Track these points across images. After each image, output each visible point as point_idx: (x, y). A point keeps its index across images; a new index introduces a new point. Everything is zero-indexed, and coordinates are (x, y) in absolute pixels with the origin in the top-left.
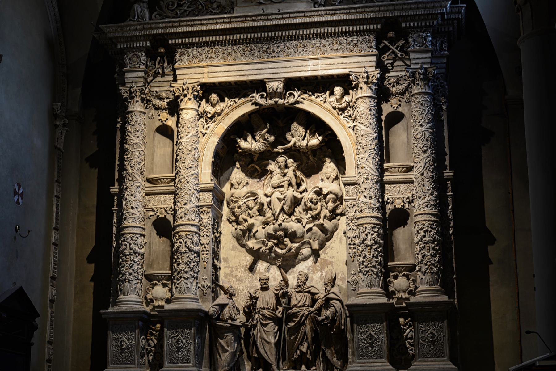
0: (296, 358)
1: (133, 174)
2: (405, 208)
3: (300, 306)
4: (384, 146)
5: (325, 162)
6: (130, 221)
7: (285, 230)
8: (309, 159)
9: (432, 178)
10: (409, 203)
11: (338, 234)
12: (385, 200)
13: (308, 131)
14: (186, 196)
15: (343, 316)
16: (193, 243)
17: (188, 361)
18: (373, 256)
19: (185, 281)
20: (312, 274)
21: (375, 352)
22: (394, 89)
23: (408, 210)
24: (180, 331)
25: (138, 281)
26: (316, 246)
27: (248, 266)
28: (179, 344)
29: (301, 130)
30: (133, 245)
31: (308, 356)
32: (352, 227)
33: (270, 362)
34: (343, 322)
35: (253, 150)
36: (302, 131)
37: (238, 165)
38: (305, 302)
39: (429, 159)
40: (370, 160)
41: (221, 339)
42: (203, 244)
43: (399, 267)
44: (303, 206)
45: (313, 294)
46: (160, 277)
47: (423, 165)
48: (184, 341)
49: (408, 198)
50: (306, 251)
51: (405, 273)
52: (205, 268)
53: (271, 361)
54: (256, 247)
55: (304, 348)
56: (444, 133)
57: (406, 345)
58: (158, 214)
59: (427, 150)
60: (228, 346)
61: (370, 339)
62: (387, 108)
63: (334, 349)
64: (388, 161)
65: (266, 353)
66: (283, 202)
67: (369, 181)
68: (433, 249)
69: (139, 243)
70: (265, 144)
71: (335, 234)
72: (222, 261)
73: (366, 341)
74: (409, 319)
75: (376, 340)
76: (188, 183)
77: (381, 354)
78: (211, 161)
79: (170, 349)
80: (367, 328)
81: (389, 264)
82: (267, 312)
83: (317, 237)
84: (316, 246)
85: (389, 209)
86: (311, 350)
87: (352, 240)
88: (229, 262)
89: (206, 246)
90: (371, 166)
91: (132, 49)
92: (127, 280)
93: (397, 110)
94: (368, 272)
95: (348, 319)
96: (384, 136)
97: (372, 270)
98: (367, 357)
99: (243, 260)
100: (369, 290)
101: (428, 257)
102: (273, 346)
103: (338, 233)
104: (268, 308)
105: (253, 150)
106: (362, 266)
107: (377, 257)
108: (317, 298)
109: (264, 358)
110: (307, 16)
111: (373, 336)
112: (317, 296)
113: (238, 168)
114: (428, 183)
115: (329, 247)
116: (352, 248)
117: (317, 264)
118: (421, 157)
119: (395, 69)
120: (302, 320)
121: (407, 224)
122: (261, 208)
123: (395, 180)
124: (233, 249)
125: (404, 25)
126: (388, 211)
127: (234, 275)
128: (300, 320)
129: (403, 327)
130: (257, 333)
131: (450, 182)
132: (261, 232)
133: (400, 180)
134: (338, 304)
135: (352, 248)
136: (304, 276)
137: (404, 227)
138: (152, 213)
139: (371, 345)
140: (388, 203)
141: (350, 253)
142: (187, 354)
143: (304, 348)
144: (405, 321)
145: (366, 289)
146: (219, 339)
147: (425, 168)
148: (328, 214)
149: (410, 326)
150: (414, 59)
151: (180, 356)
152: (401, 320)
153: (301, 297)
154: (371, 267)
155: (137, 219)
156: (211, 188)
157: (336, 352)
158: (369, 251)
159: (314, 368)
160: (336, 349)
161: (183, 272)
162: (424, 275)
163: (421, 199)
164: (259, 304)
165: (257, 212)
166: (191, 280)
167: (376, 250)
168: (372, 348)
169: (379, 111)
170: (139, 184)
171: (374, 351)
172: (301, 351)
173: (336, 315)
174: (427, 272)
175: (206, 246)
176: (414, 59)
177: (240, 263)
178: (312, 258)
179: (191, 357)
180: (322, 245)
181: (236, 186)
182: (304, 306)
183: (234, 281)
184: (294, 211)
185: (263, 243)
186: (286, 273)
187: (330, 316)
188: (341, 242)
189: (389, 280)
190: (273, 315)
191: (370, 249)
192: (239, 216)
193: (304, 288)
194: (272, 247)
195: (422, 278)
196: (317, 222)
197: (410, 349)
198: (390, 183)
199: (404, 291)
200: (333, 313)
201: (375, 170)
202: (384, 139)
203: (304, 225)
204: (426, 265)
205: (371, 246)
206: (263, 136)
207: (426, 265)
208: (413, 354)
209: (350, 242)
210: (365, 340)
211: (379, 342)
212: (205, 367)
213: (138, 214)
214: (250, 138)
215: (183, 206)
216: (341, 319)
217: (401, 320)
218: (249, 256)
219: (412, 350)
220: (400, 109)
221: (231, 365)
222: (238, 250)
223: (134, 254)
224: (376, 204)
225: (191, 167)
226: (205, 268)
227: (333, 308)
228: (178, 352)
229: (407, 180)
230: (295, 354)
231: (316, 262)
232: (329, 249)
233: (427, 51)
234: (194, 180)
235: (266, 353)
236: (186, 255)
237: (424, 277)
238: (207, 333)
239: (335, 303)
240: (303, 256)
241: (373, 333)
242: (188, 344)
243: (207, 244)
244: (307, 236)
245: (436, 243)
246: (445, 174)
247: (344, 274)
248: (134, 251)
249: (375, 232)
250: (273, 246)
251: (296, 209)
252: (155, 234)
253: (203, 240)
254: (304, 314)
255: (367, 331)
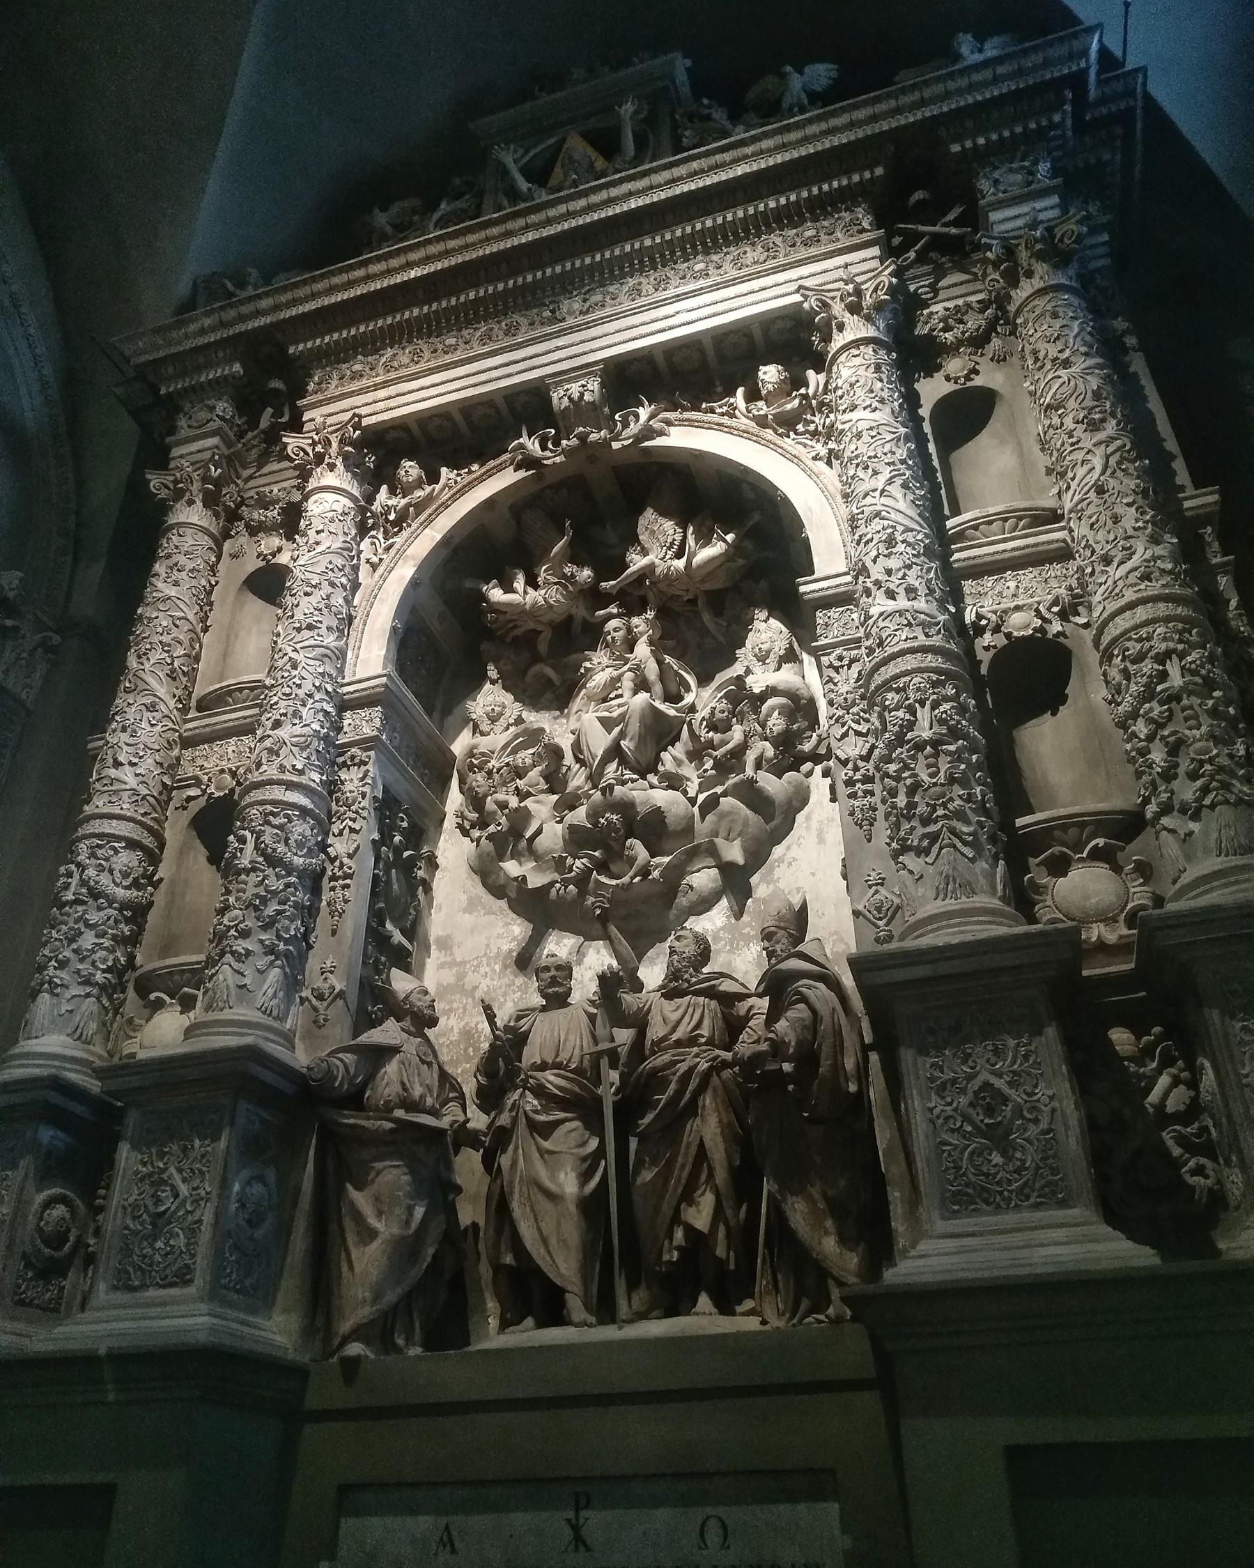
0: (670, 1262)
1: (141, 674)
2: (1050, 636)
3: (678, 1043)
4: (940, 479)
5: (751, 621)
6: (100, 804)
7: (626, 808)
8: (704, 632)
9: (1145, 493)
10: (1064, 616)
11: (808, 818)
12: (967, 621)
13: (691, 529)
14: (282, 704)
15: (850, 1041)
16: (287, 840)
17: (183, 1279)
18: (951, 780)
19: (236, 965)
20: (729, 952)
21: (1027, 1175)
22: (949, 336)
23: (1062, 639)
24: (175, 1147)
25: (88, 989)
26: (734, 853)
27: (515, 954)
28: (158, 1201)
29: (668, 527)
30: (91, 872)
31: (720, 1251)
32: (853, 725)
33: (558, 1281)
34: (850, 1064)
35: (527, 607)
36: (672, 532)
37: (493, 673)
38: (699, 1025)
39: (1118, 443)
40: (896, 490)
41: (359, 1188)
42: (336, 858)
43: (1064, 828)
44: (685, 744)
45: (728, 1000)
46: (177, 977)
47: (1098, 462)
48: (184, 1190)
49: (1055, 602)
50: (703, 878)
51: (1101, 841)
52: (334, 933)
53: (561, 1276)
54: (536, 881)
55: (701, 1215)
56: (1149, 406)
57: (1166, 1152)
58: (212, 789)
59: (1103, 420)
60: (380, 1214)
61: (990, 1111)
62: (932, 390)
63: (824, 1195)
64: (956, 512)
65: (545, 1241)
66: (617, 730)
67: (901, 547)
68: (1214, 713)
69: (117, 867)
70: (565, 587)
71: (800, 818)
72: (433, 947)
73: (972, 1123)
74: (1156, 1030)
75: (1018, 1112)
76: (295, 667)
77: (1055, 1184)
78: (388, 627)
79: (127, 1228)
80: (964, 1062)
81: (1019, 822)
82: (552, 1078)
83: (738, 828)
84: (734, 853)
85: (987, 649)
86: (732, 1223)
87: (856, 769)
88: (455, 948)
89: (346, 860)
90: (902, 505)
91: (197, 392)
92: (46, 986)
93: (969, 384)
94: (934, 837)
95: (874, 1057)
96: (935, 457)
97: (953, 831)
98: (988, 1204)
99: (499, 936)
100: (950, 904)
101: (1198, 745)
102: (572, 1208)
103: (810, 813)
104: (557, 1066)
105: (527, 607)
106: (906, 826)
107: (964, 782)
108: (743, 1012)
109: (538, 1271)
110: (661, 186)
111: (999, 1092)
112: (742, 1008)
113: (493, 682)
114: (1133, 510)
115: (781, 860)
116: (860, 793)
117: (746, 918)
118: (1087, 443)
119: (943, 295)
120: (688, 1095)
121: (1063, 699)
122: (552, 769)
123: (997, 557)
124: (471, 907)
125: (956, 148)
126: (985, 657)
127: (468, 987)
128: (680, 1092)
129: (1133, 1068)
130: (514, 1163)
131: (1209, 530)
132: (552, 835)
133: (1016, 553)
134: (819, 993)
135: (860, 793)
136: (691, 940)
137: (1054, 714)
138: (193, 792)
139: (999, 1137)
140: (980, 631)
141: (852, 814)
142: (187, 1245)
143: (701, 1215)
144: (1138, 1038)
145: (939, 902)
146: (349, 1186)
147: (1109, 472)
148: (770, 752)
149: (1167, 1062)
150: (1000, 222)
151: (158, 1258)
152: (1120, 1037)
153: (681, 1011)
154: (945, 817)
155: (125, 795)
156: (378, 690)
157: (837, 1209)
158: (932, 760)
159: (749, 1304)
160: (830, 1193)
161: (232, 932)
162: (1196, 817)
163: (1115, 564)
164: (531, 1055)
165: (542, 781)
166: (262, 962)
167: (957, 757)
168: (1004, 1154)
169: (911, 400)
170: (152, 699)
171: (1018, 1171)
172: (690, 1230)
173: (815, 1032)
174: (1207, 802)
175: (346, 860)
176: (1000, 222)
177: (488, 946)
178: (724, 902)
179: (199, 1259)
180: (758, 856)
181: (485, 727)
182: (692, 1041)
183: (465, 1009)
184: (658, 759)
185: (560, 864)
186: (640, 957)
187: (791, 1039)
188: (821, 840)
189: (1031, 880)
190: (577, 1089)
191: (936, 755)
192: (486, 796)
193: (694, 980)
194: (587, 872)
195: (1191, 833)
196: (733, 780)
197: (1192, 1164)
198: (980, 571)
199: (1110, 920)
200: (805, 1027)
201: (917, 518)
202: (936, 463)
203: (692, 793)
204: (1193, 776)
205: (936, 743)
206: (556, 570)
207: (1193, 776)
208: (1210, 1190)
209: (851, 773)
210: (966, 1118)
211: (1036, 1121)
212: (285, 1311)
213: (132, 782)
214: (519, 584)
215: (271, 733)
216: (839, 1048)
217: (1120, 1037)
218: (519, 921)
219: (1199, 1171)
220: (978, 381)
221: (391, 1297)
222: (484, 908)
223: (91, 901)
224: (936, 613)
225: (310, 627)
226: (334, 933)
227: (802, 1006)
228: (155, 1240)
229: (1040, 548)
230: (666, 1243)
231: (739, 914)
232: (784, 866)
233: (1043, 193)
234: (318, 663)
235: (545, 1241)
236: (253, 878)
237: (1194, 826)
238: (310, 1167)
239: (809, 987)
240: (692, 896)
241: (998, 1083)
242: (196, 1202)
243: (350, 856)
244: (703, 828)
245: (1217, 694)
246: (1187, 504)
247: (841, 940)
248: (90, 890)
249: (947, 699)
250: (590, 871)
251: (665, 756)
252: (204, 859)
253: (337, 845)
254: (691, 1069)
255: (970, 1078)
